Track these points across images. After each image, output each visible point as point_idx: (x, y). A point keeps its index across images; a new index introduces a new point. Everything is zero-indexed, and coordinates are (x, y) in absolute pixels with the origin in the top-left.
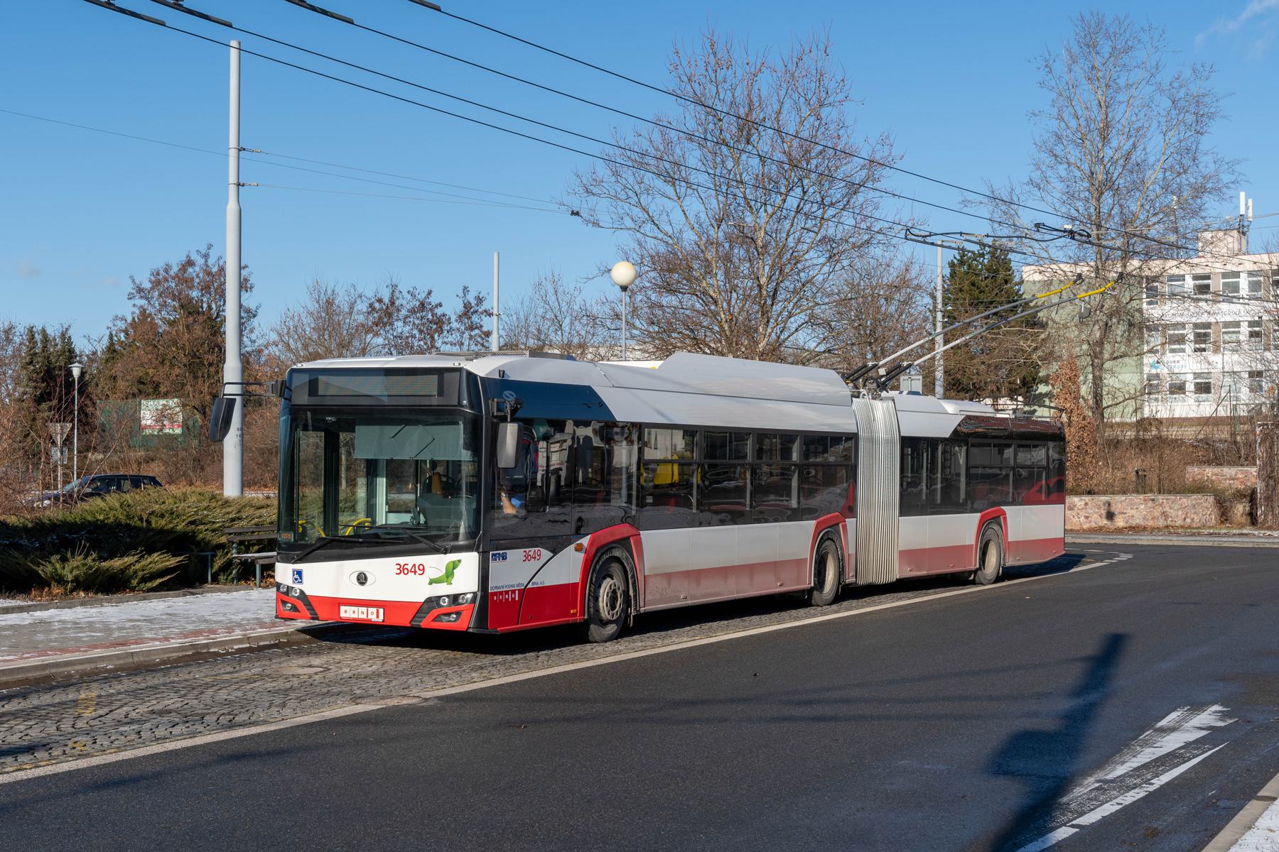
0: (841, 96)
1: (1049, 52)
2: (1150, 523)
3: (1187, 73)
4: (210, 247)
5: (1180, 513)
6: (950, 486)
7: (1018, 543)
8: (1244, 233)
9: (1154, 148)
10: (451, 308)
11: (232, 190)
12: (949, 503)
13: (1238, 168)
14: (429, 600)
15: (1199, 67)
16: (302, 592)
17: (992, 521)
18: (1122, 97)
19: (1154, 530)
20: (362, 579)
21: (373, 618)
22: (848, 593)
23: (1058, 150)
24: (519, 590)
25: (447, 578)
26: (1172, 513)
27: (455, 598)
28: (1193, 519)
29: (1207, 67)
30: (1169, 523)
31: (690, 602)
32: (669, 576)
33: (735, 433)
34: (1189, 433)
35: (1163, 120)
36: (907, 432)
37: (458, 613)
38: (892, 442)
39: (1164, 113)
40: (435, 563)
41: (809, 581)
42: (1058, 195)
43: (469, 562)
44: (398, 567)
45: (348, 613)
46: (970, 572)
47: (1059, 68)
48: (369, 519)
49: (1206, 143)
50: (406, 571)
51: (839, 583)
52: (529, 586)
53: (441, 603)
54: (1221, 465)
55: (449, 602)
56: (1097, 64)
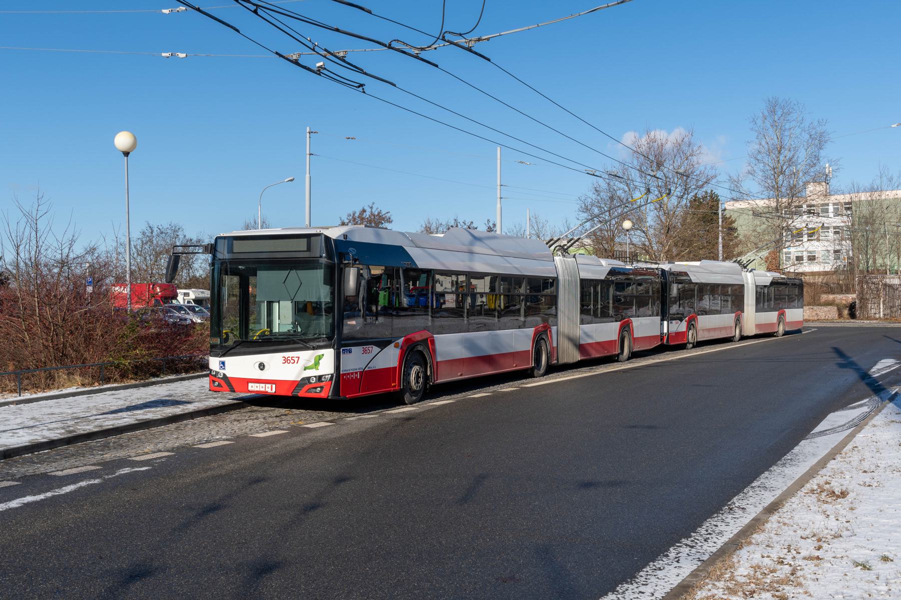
0: (698, 152)
1: (754, 115)
2: (811, 318)
3: (816, 124)
4: (373, 203)
5: (823, 314)
6: (605, 308)
7: (789, 322)
8: (828, 184)
9: (802, 156)
10: (482, 228)
11: (499, 199)
12: (603, 315)
13: (838, 163)
14: (303, 379)
15: (821, 120)
16: (224, 374)
17: (782, 315)
18: (786, 133)
19: (813, 321)
20: (262, 366)
21: (269, 390)
22: (553, 369)
23: (759, 157)
24: (360, 372)
25: (315, 366)
26: (820, 314)
27: (320, 378)
28: (828, 317)
29: (825, 121)
30: (819, 318)
31: (708, 339)
32: (703, 330)
33: (514, 278)
34: (819, 280)
35: (805, 143)
36: (585, 275)
37: (321, 387)
38: (576, 282)
39: (806, 141)
40: (306, 356)
41: (618, 351)
42: (759, 177)
43: (328, 355)
44: (284, 359)
45: (253, 387)
46: (775, 333)
47: (759, 122)
48: (269, 329)
49: (823, 153)
50: (289, 361)
51: (630, 351)
52: (366, 369)
53: (311, 381)
54: (834, 294)
55: (316, 381)
56: (776, 119)
